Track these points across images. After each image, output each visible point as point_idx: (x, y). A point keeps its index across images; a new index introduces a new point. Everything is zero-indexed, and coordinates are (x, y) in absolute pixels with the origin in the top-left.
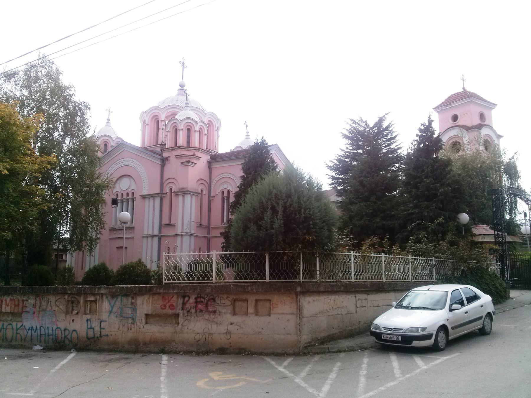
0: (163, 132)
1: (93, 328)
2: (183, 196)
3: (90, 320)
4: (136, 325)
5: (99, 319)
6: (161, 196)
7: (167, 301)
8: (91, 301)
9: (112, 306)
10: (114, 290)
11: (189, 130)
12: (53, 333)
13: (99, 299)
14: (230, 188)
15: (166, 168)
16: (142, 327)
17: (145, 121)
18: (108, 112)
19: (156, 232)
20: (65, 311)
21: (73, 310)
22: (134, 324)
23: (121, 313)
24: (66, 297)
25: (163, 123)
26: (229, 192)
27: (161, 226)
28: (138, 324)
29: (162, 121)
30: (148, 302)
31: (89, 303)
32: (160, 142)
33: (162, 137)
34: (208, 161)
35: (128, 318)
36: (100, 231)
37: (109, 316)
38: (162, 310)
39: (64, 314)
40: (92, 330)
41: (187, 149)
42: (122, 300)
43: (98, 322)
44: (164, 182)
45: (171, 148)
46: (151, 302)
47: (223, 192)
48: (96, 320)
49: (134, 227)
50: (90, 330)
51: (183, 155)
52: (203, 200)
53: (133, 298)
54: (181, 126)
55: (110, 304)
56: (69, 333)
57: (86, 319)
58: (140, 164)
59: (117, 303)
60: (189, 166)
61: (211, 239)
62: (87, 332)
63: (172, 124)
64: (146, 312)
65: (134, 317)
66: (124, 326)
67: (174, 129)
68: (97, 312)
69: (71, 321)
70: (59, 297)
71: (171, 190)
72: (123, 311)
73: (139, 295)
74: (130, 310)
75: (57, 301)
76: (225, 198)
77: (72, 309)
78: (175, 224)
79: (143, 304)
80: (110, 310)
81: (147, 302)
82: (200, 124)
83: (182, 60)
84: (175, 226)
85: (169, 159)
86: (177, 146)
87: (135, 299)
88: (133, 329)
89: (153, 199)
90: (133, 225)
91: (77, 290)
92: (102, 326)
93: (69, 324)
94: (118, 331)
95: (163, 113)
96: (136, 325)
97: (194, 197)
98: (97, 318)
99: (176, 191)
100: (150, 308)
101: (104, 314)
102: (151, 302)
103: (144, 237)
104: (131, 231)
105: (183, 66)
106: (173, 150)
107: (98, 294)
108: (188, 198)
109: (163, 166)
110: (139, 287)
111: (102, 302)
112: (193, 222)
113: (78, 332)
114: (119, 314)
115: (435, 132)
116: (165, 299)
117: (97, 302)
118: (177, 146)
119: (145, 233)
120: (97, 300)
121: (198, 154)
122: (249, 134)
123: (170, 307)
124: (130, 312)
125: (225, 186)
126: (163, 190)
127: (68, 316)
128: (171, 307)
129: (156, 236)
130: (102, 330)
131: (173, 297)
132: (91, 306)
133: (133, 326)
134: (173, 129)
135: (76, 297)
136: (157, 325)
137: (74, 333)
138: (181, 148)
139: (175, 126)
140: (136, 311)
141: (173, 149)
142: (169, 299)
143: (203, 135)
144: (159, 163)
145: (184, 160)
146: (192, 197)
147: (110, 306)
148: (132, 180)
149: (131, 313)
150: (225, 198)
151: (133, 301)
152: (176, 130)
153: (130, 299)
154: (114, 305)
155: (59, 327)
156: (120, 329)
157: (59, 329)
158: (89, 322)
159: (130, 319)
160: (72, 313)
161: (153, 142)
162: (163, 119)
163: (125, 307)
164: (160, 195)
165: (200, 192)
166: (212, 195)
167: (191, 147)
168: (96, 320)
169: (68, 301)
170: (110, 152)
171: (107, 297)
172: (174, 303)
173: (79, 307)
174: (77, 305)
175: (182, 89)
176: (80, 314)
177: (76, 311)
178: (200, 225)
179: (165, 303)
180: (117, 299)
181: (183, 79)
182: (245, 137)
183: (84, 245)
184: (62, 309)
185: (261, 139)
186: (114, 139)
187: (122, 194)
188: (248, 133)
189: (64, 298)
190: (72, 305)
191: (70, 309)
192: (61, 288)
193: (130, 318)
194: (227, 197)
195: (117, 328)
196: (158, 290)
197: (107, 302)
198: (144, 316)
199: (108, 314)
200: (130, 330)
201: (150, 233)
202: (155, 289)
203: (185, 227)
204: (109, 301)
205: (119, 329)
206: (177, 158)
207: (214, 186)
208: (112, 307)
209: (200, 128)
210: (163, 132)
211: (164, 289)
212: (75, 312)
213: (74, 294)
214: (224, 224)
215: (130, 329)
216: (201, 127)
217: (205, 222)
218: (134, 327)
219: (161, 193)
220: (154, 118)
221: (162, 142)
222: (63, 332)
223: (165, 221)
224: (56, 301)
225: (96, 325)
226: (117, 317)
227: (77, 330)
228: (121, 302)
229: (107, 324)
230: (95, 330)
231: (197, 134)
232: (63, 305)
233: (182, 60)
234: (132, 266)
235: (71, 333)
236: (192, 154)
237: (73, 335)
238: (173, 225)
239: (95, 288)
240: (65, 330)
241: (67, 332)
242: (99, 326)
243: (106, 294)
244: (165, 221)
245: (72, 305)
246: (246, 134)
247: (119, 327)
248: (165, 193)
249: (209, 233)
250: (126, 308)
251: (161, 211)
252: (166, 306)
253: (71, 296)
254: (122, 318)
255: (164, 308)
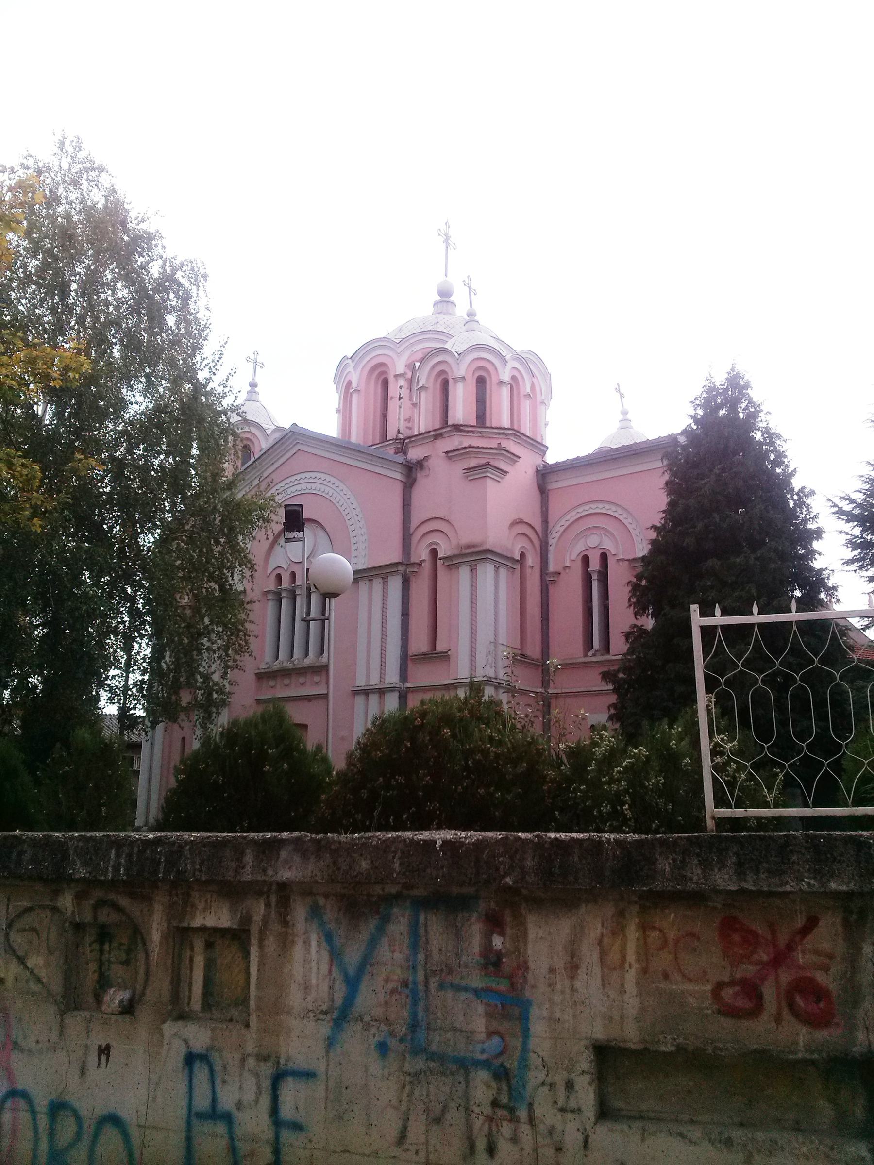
0: (400, 407)
1: (227, 1118)
2: (473, 569)
3: (204, 1058)
4: (531, 1120)
5: (263, 1058)
6: (406, 570)
7: (764, 956)
8: (215, 930)
9: (351, 971)
10: (365, 865)
11: (481, 382)
12: (488, 428)
13: (265, 922)
14: (608, 545)
15: (418, 494)
16: (572, 1137)
17: (350, 383)
18: (251, 365)
19: (392, 678)
20: (57, 987)
21: (103, 983)
22: (512, 1110)
23: (414, 1026)
24: (66, 901)
25: (402, 382)
26: (604, 557)
27: (406, 659)
28: (545, 1112)
29: (396, 376)
30: (614, 957)
31: (199, 944)
32: (391, 434)
33: (399, 419)
34: (537, 471)
35: (465, 1065)
36: (235, 661)
37: (330, 1043)
38: (728, 1023)
39: (52, 1010)
40: (221, 1128)
41: (481, 432)
42: (416, 939)
43: (257, 1075)
44: (412, 530)
45: (432, 433)
46: (631, 957)
47: (586, 560)
48: (243, 1060)
49: (325, 668)
50: (208, 1127)
51: (470, 447)
52: (528, 582)
53: (494, 923)
54: (461, 369)
55: (335, 955)
56: (78, 1135)
57: (183, 1050)
58: (342, 486)
59: (384, 951)
60: (489, 480)
61: (553, 701)
62: (189, 1139)
63: (434, 367)
64: (599, 1033)
65: (512, 1064)
66: (438, 1121)
67: (440, 380)
68: (252, 1004)
69: (93, 1058)
70: (26, 904)
71: (434, 552)
72: (427, 1009)
73: (537, 903)
74: (481, 1009)
75: (18, 925)
76: (595, 577)
77: (101, 975)
78: (449, 653)
79: (573, 968)
80: (339, 1001)
81: (603, 954)
82: (512, 364)
83: (443, 227)
84: (448, 657)
85: (425, 464)
86: (450, 423)
87: (509, 931)
88: (504, 1147)
89: (380, 580)
90: (324, 659)
91: (130, 855)
92: (287, 1112)
93: (83, 1071)
94: (395, 1151)
95: (399, 355)
96: (531, 1120)
97: (503, 572)
98: (250, 1047)
99: (449, 554)
100: (632, 1003)
101: (294, 1023)
102: (631, 957)
103: (356, 693)
104: (317, 679)
105: (447, 241)
106: (436, 437)
107: (259, 889)
108: (487, 572)
109: (409, 484)
110: (540, 846)
111: (285, 943)
112: (501, 648)
113: (134, 1133)
114: (402, 1030)
115: (817, 556)
116: (751, 939)
117: (254, 941)
118: (450, 423)
119: (361, 682)
120: (254, 929)
121: (512, 446)
122: (629, 416)
123: (791, 1006)
124: (480, 1025)
125: (593, 541)
126: (409, 554)
127: (75, 1022)
128: (799, 1001)
129: (392, 689)
130: (286, 1135)
131: (812, 923)
132: (209, 965)
133: (506, 1129)
134: (436, 380)
135: (124, 902)
136: (696, 1133)
137: (111, 1137)
138: (461, 431)
139: (443, 372)
140: (524, 1018)
141: (437, 435)
142: (783, 940)
143: (522, 398)
144: (398, 476)
145: (473, 463)
146: (497, 569)
147: (336, 973)
148: (321, 533)
149: (490, 1034)
150: (595, 577)
151: (497, 942)
152: (445, 385)
153: (475, 931)
154: (361, 969)
155: (20, 1087)
156: (411, 1137)
157: (22, 1103)
158: (201, 1074)
159: (482, 1076)
160: (98, 1001)
161: (373, 437)
162: (400, 369)
163: (441, 987)
164: (401, 568)
165: (518, 557)
166: (552, 568)
167: (488, 424)
168: (243, 1060)
169: (78, 927)
170: (259, 458)
171: (315, 912)
172: (826, 969)
173: (142, 971)
174: (129, 952)
175: (445, 299)
176: (145, 1014)
177: (124, 995)
178: (520, 658)
179: (748, 970)
180: (381, 930)
181: (446, 275)
182: (618, 425)
183: (184, 703)
184: (43, 973)
185: (729, 373)
186: (269, 432)
187: (293, 574)
188: (625, 413)
189: (55, 909)
190: (102, 951)
191: (90, 978)
192: (34, 842)
193: (486, 1064)
194: (599, 572)
195: (393, 1134)
196: (695, 872)
197: (314, 943)
198: (585, 1061)
199: (325, 1029)
200: (481, 1155)
201: (374, 681)
202: (665, 865)
203: (481, 659)
204: (329, 937)
205: (402, 1138)
206: (450, 458)
207: (557, 544)
208: (353, 984)
209: (514, 378)
210: (400, 407)
211: (740, 864)
212: (116, 997)
213: (113, 885)
214: (594, 655)
215: (481, 1144)
216: (516, 374)
217: (534, 650)
218: (514, 1140)
219: (405, 562)
220: (377, 372)
221: (399, 432)
222: (43, 1121)
223: (419, 644)
224: (10, 926)
225: (249, 1096)
226: (383, 1048)
227: (124, 1114)
228: (414, 947)
229: (320, 1092)
230: (239, 1131)
231: (505, 391)
232: (50, 952)
233: (443, 227)
234: (447, 719)
235: (89, 1126)
236: (496, 446)
237: (99, 1150)
238: (444, 657)
239: (238, 850)
240: (57, 1108)
241: (67, 1130)
242: (265, 1102)
243: (307, 890)
244: (419, 644)
245: (102, 951)
246: (621, 417)
247: (405, 1127)
248: (417, 561)
249: (545, 683)
250: (450, 994)
251: (405, 614)
252: (760, 997)
253: (98, 894)
254: (421, 1063)
255: (742, 1003)
